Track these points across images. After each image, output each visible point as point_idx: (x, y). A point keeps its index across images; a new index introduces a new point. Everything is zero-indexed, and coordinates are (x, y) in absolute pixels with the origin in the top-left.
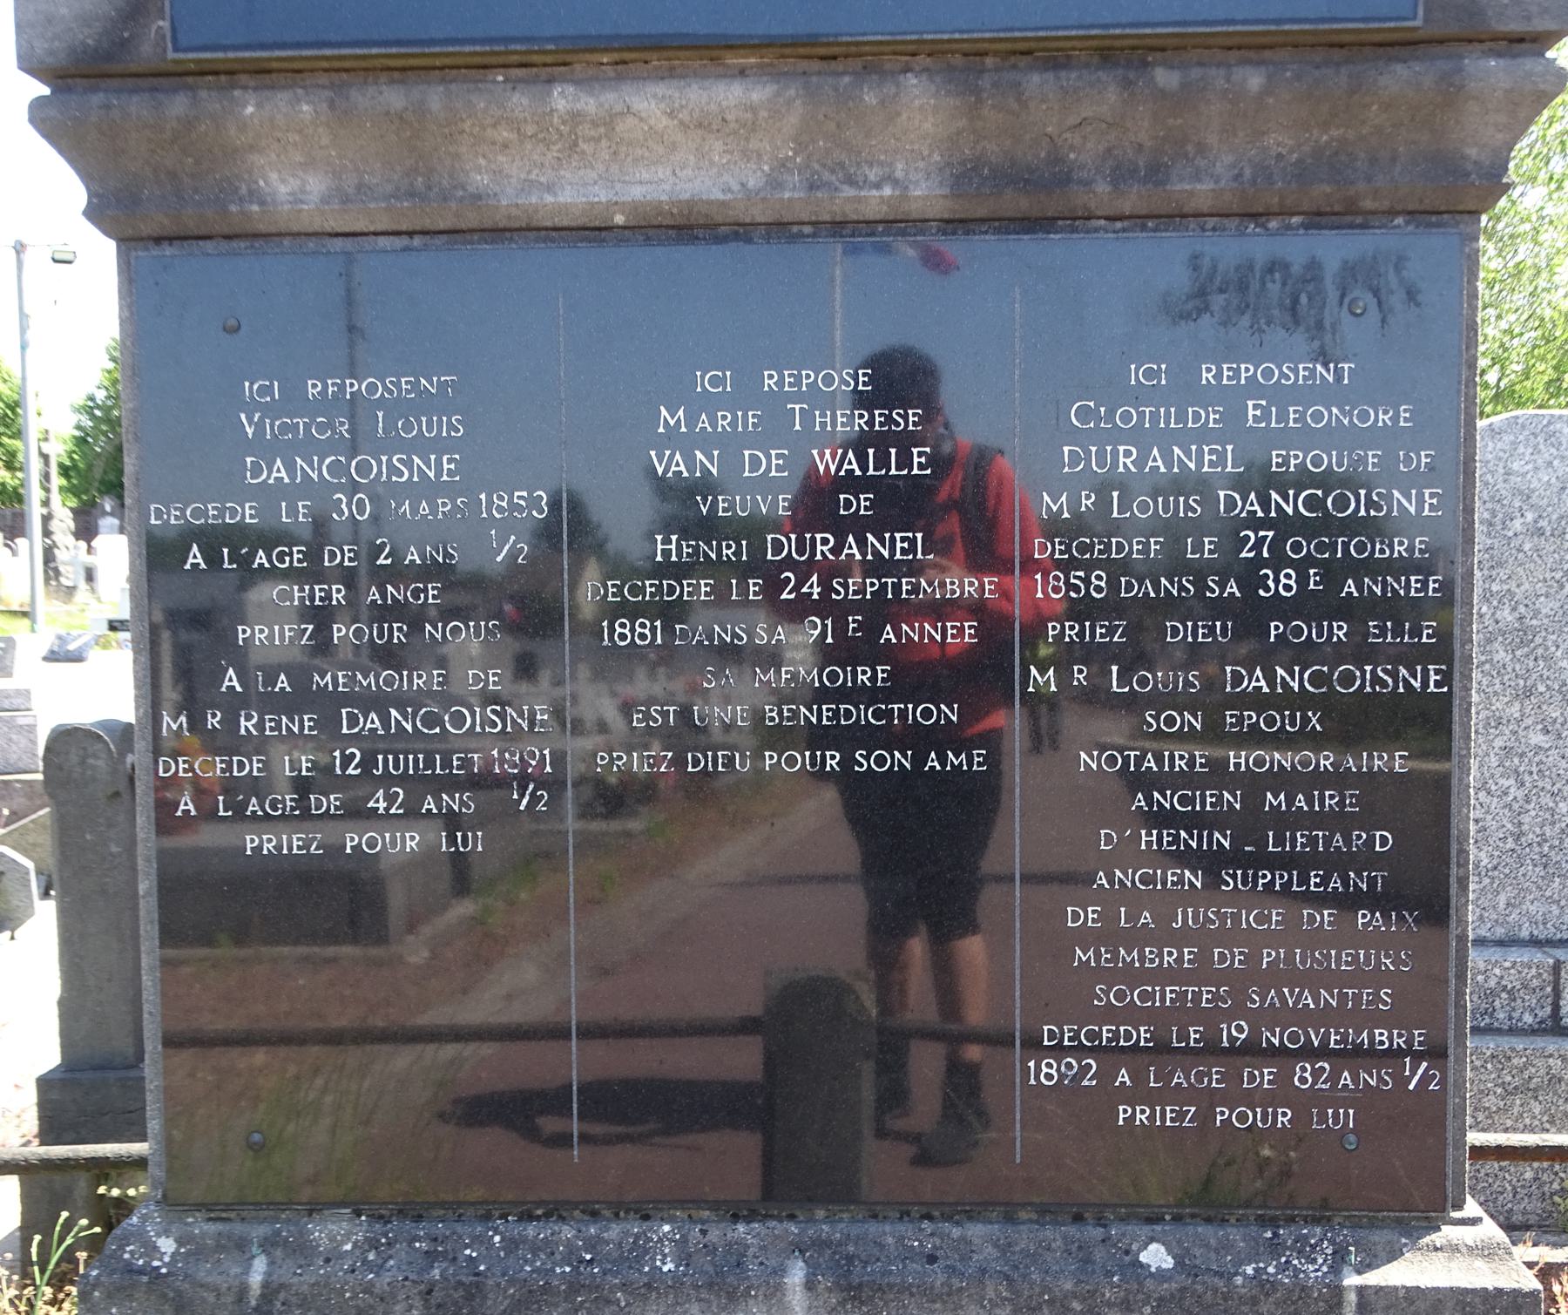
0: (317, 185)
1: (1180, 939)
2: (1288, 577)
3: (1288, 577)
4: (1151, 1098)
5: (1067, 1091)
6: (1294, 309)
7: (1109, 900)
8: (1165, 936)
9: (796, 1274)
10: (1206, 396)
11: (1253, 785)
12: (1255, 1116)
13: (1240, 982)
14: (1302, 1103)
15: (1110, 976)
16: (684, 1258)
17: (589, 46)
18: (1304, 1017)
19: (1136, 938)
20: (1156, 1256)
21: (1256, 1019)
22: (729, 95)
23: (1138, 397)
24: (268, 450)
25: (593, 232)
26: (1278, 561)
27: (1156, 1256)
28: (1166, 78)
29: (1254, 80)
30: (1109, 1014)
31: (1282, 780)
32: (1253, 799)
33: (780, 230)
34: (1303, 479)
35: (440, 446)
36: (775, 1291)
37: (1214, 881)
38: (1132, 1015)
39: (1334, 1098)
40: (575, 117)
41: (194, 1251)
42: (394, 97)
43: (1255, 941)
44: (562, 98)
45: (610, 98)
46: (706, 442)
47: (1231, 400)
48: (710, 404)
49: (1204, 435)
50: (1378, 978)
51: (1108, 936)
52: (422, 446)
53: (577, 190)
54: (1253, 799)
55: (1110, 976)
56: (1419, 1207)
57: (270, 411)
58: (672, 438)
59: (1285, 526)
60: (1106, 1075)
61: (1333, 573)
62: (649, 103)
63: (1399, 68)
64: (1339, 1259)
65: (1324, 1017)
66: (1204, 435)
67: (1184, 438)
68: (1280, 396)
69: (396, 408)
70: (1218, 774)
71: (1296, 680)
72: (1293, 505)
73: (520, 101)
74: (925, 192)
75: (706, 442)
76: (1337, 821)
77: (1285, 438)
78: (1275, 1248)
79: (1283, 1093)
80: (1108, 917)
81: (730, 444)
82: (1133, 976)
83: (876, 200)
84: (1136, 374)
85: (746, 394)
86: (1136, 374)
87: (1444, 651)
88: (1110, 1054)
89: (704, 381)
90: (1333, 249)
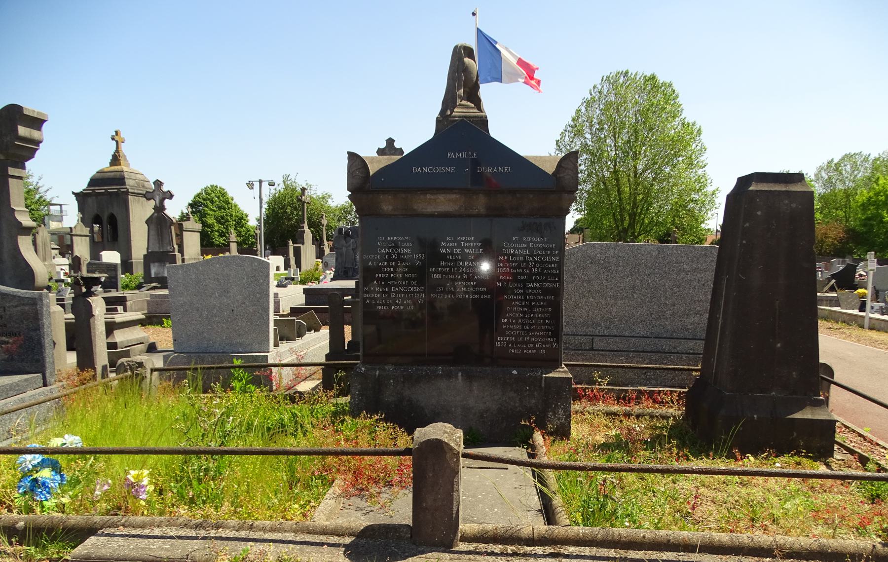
0: (390, 208)
1: (519, 324)
2: (536, 270)
3: (536, 270)
4: (515, 349)
5: (502, 347)
6: (537, 230)
7: (508, 318)
8: (516, 324)
9: (460, 374)
10: (524, 242)
11: (530, 301)
12: (530, 351)
13: (528, 331)
14: (537, 349)
15: (508, 330)
16: (442, 371)
17: (443, 189)
18: (538, 336)
19: (513, 324)
20: (515, 372)
21: (531, 337)
22: (454, 196)
23: (514, 242)
24: (382, 248)
25: (432, 216)
26: (535, 267)
27: (515, 372)
28: (518, 195)
29: (531, 196)
30: (508, 336)
31: (534, 300)
32: (530, 303)
33: (460, 216)
34: (538, 255)
35: (408, 247)
36: (457, 377)
37: (524, 315)
38: (512, 336)
39: (543, 349)
40: (430, 199)
41: (367, 370)
42: (403, 196)
43: (531, 325)
44: (428, 196)
45: (436, 196)
46: (449, 247)
47: (528, 243)
48: (450, 242)
49: (524, 248)
50: (549, 331)
51: (508, 323)
52: (405, 247)
53: (430, 209)
54: (530, 303)
55: (508, 330)
56: (555, 364)
57: (383, 241)
58: (444, 247)
59: (536, 262)
60: (508, 344)
61: (543, 269)
62: (441, 198)
63: (47, 351)
64: (542, 374)
65: (541, 336)
66: (524, 248)
67: (521, 248)
68: (535, 243)
69: (402, 241)
70: (525, 300)
71: (537, 285)
72: (537, 259)
73: (422, 196)
74: (483, 211)
75: (449, 247)
76: (542, 306)
77: (536, 249)
78: (533, 371)
79: (534, 348)
80: (508, 321)
81: (452, 248)
82: (512, 330)
83: (475, 212)
84: (514, 239)
85: (455, 240)
86: (514, 239)
87: (560, 282)
88: (508, 342)
89: (448, 238)
90: (544, 221)
